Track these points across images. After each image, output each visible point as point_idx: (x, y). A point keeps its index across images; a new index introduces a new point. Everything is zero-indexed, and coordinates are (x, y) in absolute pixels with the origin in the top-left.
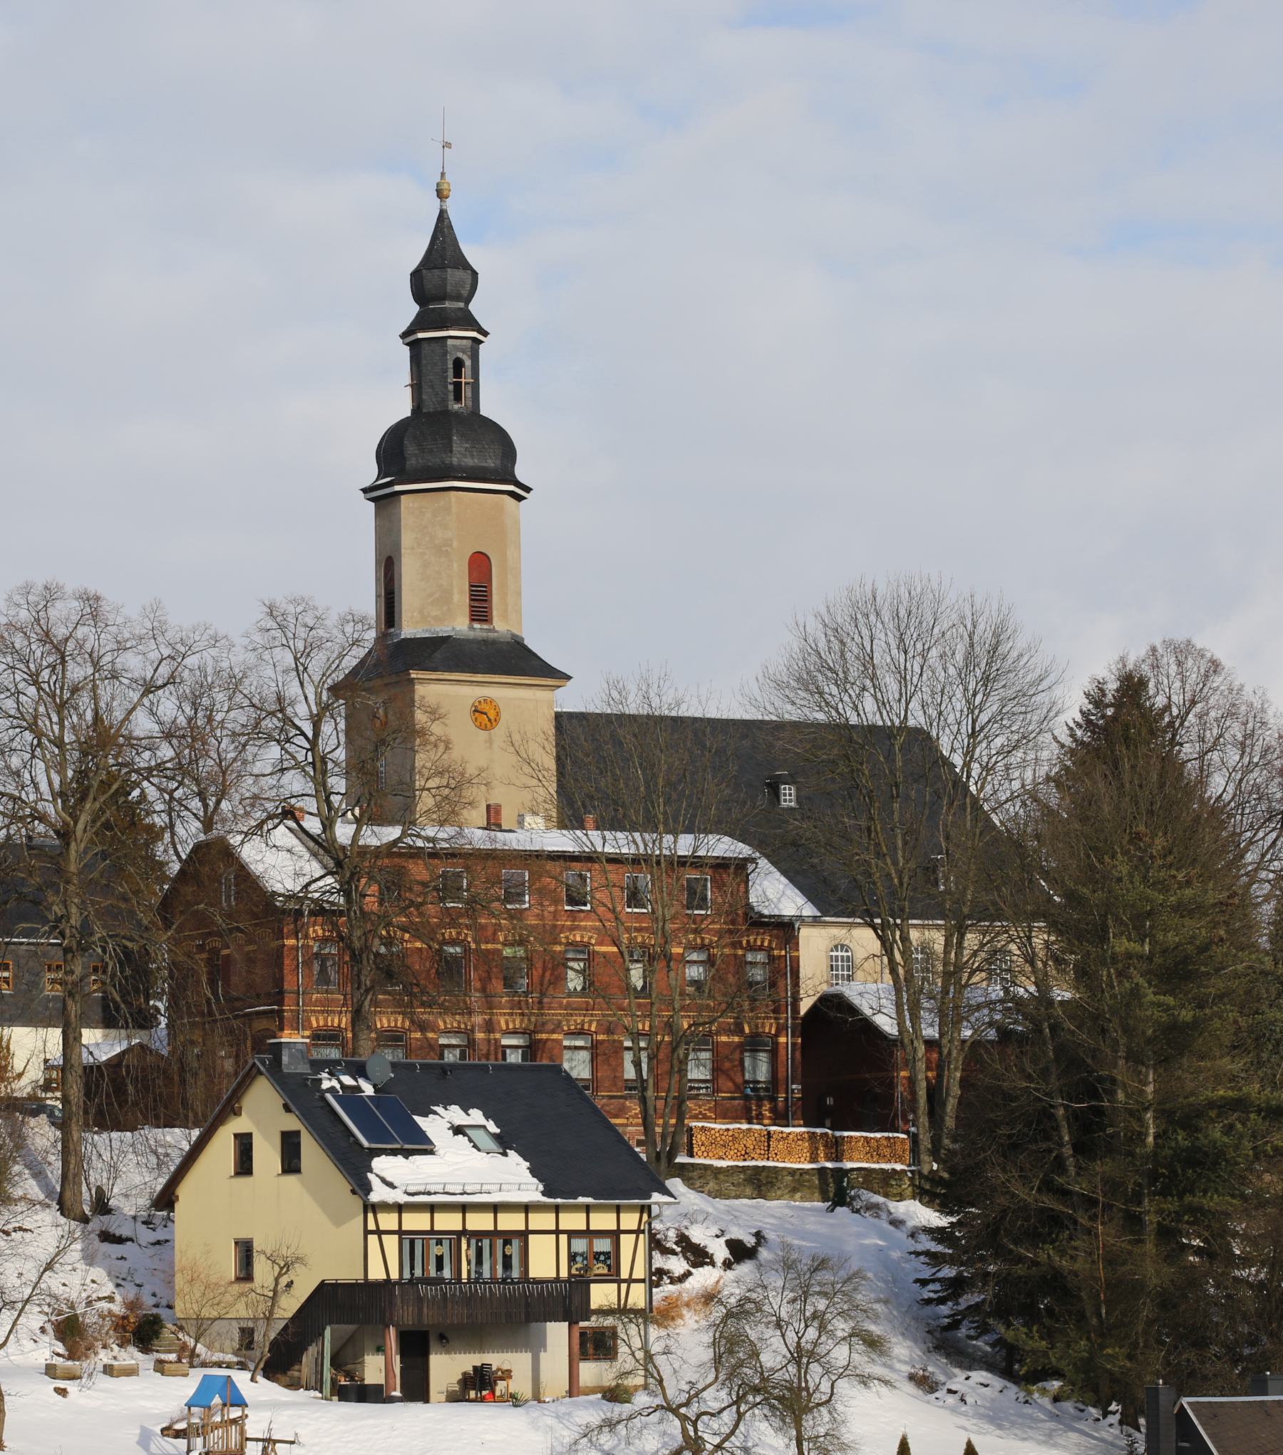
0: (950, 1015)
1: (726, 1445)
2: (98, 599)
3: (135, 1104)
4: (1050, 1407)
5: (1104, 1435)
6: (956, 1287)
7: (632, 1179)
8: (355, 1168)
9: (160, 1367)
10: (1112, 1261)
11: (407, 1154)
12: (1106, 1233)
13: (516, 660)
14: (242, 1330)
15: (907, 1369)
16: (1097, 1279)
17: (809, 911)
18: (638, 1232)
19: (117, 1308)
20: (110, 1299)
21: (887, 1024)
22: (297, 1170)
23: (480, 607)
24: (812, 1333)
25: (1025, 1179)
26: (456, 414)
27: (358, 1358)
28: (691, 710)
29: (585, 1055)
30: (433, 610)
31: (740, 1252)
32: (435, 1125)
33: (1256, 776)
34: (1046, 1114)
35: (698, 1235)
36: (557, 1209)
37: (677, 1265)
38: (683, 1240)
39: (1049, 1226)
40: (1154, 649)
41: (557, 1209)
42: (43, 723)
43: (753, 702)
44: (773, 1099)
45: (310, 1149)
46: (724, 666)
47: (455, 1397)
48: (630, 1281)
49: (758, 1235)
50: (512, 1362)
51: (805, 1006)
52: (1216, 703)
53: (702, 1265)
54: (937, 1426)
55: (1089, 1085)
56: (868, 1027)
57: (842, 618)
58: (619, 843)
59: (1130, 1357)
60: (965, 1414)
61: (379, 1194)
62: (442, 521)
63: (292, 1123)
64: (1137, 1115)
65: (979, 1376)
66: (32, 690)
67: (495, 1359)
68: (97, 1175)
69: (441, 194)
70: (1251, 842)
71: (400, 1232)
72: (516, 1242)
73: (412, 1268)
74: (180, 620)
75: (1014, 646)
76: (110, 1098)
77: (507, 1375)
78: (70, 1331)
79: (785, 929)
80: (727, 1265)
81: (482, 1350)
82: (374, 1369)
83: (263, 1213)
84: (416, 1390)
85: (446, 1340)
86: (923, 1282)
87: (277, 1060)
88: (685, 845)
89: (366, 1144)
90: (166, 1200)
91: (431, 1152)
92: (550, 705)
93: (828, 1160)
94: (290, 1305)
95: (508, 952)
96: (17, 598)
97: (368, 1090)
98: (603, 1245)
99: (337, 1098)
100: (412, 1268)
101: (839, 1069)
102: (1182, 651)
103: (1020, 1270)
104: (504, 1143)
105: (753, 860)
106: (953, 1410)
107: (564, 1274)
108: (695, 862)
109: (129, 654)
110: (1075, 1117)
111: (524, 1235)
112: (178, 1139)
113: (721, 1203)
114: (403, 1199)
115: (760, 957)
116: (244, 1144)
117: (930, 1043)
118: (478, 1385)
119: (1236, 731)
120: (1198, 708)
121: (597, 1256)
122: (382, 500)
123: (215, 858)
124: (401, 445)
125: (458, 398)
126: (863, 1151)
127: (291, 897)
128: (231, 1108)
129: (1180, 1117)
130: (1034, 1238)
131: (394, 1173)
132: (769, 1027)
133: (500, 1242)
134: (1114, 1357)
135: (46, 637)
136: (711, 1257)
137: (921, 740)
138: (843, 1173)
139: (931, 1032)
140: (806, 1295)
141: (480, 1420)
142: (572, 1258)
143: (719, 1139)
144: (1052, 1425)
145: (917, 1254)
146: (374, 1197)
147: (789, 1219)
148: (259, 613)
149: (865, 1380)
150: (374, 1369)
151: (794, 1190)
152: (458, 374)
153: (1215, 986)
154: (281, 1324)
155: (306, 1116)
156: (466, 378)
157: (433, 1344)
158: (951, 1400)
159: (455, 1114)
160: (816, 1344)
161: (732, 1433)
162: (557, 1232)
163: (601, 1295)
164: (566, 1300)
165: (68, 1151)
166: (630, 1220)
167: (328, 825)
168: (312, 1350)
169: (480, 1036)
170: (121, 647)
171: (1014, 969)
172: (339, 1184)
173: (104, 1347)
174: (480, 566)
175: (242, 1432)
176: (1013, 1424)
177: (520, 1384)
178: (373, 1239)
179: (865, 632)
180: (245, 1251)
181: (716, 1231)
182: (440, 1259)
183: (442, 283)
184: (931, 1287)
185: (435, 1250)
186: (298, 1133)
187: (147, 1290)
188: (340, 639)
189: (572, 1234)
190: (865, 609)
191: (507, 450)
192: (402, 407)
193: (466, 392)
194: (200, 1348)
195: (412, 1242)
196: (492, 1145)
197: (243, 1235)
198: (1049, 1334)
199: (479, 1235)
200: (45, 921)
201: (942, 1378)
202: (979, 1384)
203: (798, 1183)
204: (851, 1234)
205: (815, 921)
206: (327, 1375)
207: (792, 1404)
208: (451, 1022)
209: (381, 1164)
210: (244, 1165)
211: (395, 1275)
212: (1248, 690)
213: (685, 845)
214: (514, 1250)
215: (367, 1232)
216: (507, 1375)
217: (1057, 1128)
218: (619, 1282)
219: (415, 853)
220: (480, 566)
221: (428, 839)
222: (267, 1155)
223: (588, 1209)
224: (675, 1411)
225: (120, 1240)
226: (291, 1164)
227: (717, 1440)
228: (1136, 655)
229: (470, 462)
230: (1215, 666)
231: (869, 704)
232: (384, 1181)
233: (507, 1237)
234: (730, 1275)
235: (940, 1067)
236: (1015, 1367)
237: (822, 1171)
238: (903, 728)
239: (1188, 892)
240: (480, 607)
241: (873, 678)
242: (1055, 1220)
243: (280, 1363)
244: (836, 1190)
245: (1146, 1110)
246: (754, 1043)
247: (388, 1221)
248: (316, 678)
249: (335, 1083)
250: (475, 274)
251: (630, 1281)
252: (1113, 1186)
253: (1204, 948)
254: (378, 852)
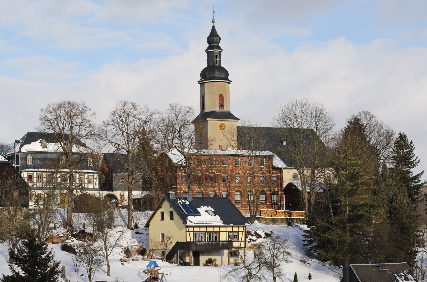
0: (312, 186)
1: (257, 274)
2: (135, 104)
3: (143, 206)
4: (329, 266)
5: (339, 272)
6: (311, 242)
7: (241, 221)
8: (184, 219)
9: (144, 259)
10: (339, 236)
11: (195, 216)
12: (338, 231)
13: (229, 116)
14: (163, 252)
15: (300, 259)
16: (337, 240)
17: (285, 166)
18: (243, 231)
19: (137, 247)
20: (137, 245)
21: (300, 188)
22: (173, 219)
23: (221, 105)
24: (276, 252)
25: (323, 220)
26: (216, 66)
27: (185, 257)
28: (259, 126)
29: (239, 196)
30: (212, 106)
31: (267, 235)
32: (202, 210)
33: (381, 138)
34: (328, 207)
35: (259, 232)
36: (226, 227)
37: (254, 238)
38: (256, 233)
39: (327, 230)
40: (360, 113)
41: (226, 227)
42: (124, 129)
43: (272, 124)
44: (277, 204)
45: (175, 215)
46: (266, 117)
47: (205, 265)
48: (241, 241)
49: (271, 232)
50: (217, 258)
51: (284, 186)
52: (373, 123)
53: (259, 238)
54: (303, 271)
55: (336, 201)
56: (298, 189)
57: (290, 107)
58: (244, 152)
59: (343, 256)
60: (310, 268)
61: (189, 224)
62: (214, 88)
63: (172, 210)
64: (345, 207)
65: (314, 260)
66: (121, 123)
67: (213, 257)
68: (136, 221)
69: (213, 22)
70: (380, 152)
71: (193, 232)
72: (217, 233)
73: (196, 238)
74: (151, 108)
75: (325, 112)
76: (139, 205)
77: (215, 260)
78: (127, 252)
79: (280, 170)
80: (264, 238)
81: (210, 255)
82: (187, 260)
83: (166, 228)
84: (197, 263)
85: (203, 253)
86: (304, 241)
87: (169, 197)
88: (258, 153)
89: (186, 214)
90: (147, 225)
91: (200, 215)
92: (236, 125)
93: (288, 216)
94: (171, 247)
95: (223, 175)
96: (119, 104)
97: (188, 203)
98: (236, 234)
99: (181, 204)
100: (196, 238)
101: (292, 197)
102: (366, 113)
103: (323, 238)
104: (215, 213)
105: (273, 156)
106: (308, 267)
107: (227, 240)
108: (259, 156)
109: (141, 115)
110: (333, 208)
111: (219, 232)
112: (151, 213)
113: (265, 225)
114: (194, 225)
115: (275, 175)
116: (163, 213)
117: (308, 193)
118: (209, 262)
119: (377, 129)
120: (369, 125)
121: (234, 236)
122: (201, 83)
123: (164, 157)
124: (205, 73)
125: (217, 63)
126: (295, 215)
127: (177, 164)
128: (160, 207)
129: (353, 208)
130: (325, 232)
131: (192, 220)
132: (276, 189)
133: (214, 233)
134: (340, 256)
135: (124, 112)
136: (261, 236)
137: (312, 130)
138: (292, 219)
139: (308, 190)
140: (275, 243)
141: (210, 269)
142: (229, 236)
143: (266, 212)
144: (328, 270)
145: (303, 235)
146: (187, 225)
147: (278, 229)
148: (168, 106)
149: (287, 261)
150: (187, 260)
151: (281, 223)
152: (216, 58)
153: (360, 181)
154: (169, 251)
155: (174, 208)
156: (218, 59)
157: (200, 254)
158: (308, 265)
159: (205, 208)
160: (277, 254)
161: (258, 272)
162: (226, 231)
163: (236, 244)
164: (228, 245)
165: (129, 215)
166: (241, 229)
167: (183, 149)
168: (175, 255)
169: (217, 192)
170: (140, 114)
171: (325, 177)
172: (180, 222)
173: (135, 255)
174: (221, 97)
175: (158, 272)
176: (320, 270)
177: (218, 262)
178: (188, 233)
179: (295, 109)
180: (163, 235)
181: (262, 231)
182: (202, 237)
183: (213, 40)
184: (306, 242)
185: (201, 235)
186: (173, 212)
187: (145, 243)
188: (185, 112)
189: (229, 232)
190: (295, 104)
191: (227, 73)
192: (206, 66)
193: (218, 62)
194: (153, 255)
195: (196, 234)
196: (213, 214)
197: (163, 232)
198: (327, 252)
199: (210, 232)
200: (124, 169)
201: (307, 261)
202: (314, 262)
203: (282, 221)
204: (292, 231)
205: (286, 168)
206: (178, 261)
207: (271, 266)
208: (210, 189)
209: (189, 218)
210: (163, 218)
211: (192, 240)
212: (379, 121)
213: (258, 153)
214: (217, 235)
215: (186, 232)
216: (215, 260)
217: (330, 210)
218: (239, 241)
219: (201, 155)
220: (221, 97)
221: (204, 152)
222: (167, 216)
223: (232, 227)
224: (246, 268)
225: (140, 234)
226: (172, 218)
227: (255, 273)
228: (356, 113)
229: (219, 76)
230: (372, 116)
231: (295, 124)
232: (190, 221)
233: (216, 232)
234: (265, 239)
235: (310, 197)
236: (323, 259)
237: (287, 219)
238: (302, 129)
239: (355, 161)
240: (221, 105)
241: (296, 119)
242: (329, 229)
243: (169, 258)
244: (289, 223)
245: (347, 206)
246: (274, 193)
247: (191, 229)
248: (180, 119)
249: (181, 201)
250: (220, 38)
251: (241, 241)
252: (340, 221)
253: (358, 173)
254: (192, 155)
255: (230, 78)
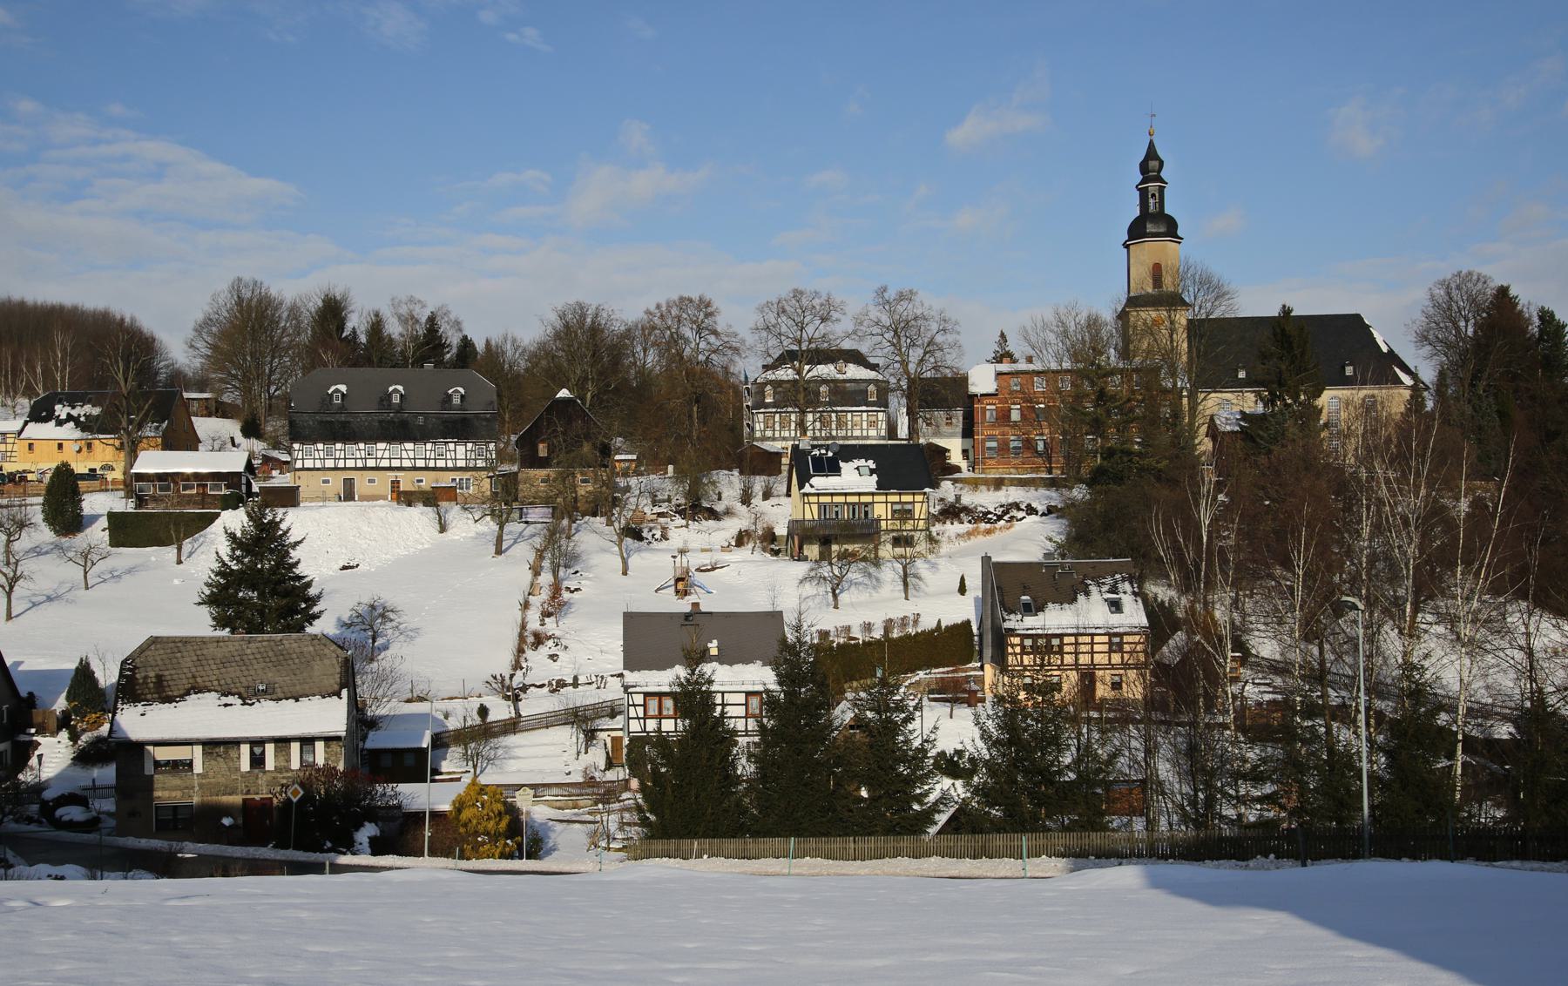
166: (919, 498)
183: (1151, 166)
199: (854, 504)
233: (866, 505)
247: (813, 499)
255: (1179, 233)
